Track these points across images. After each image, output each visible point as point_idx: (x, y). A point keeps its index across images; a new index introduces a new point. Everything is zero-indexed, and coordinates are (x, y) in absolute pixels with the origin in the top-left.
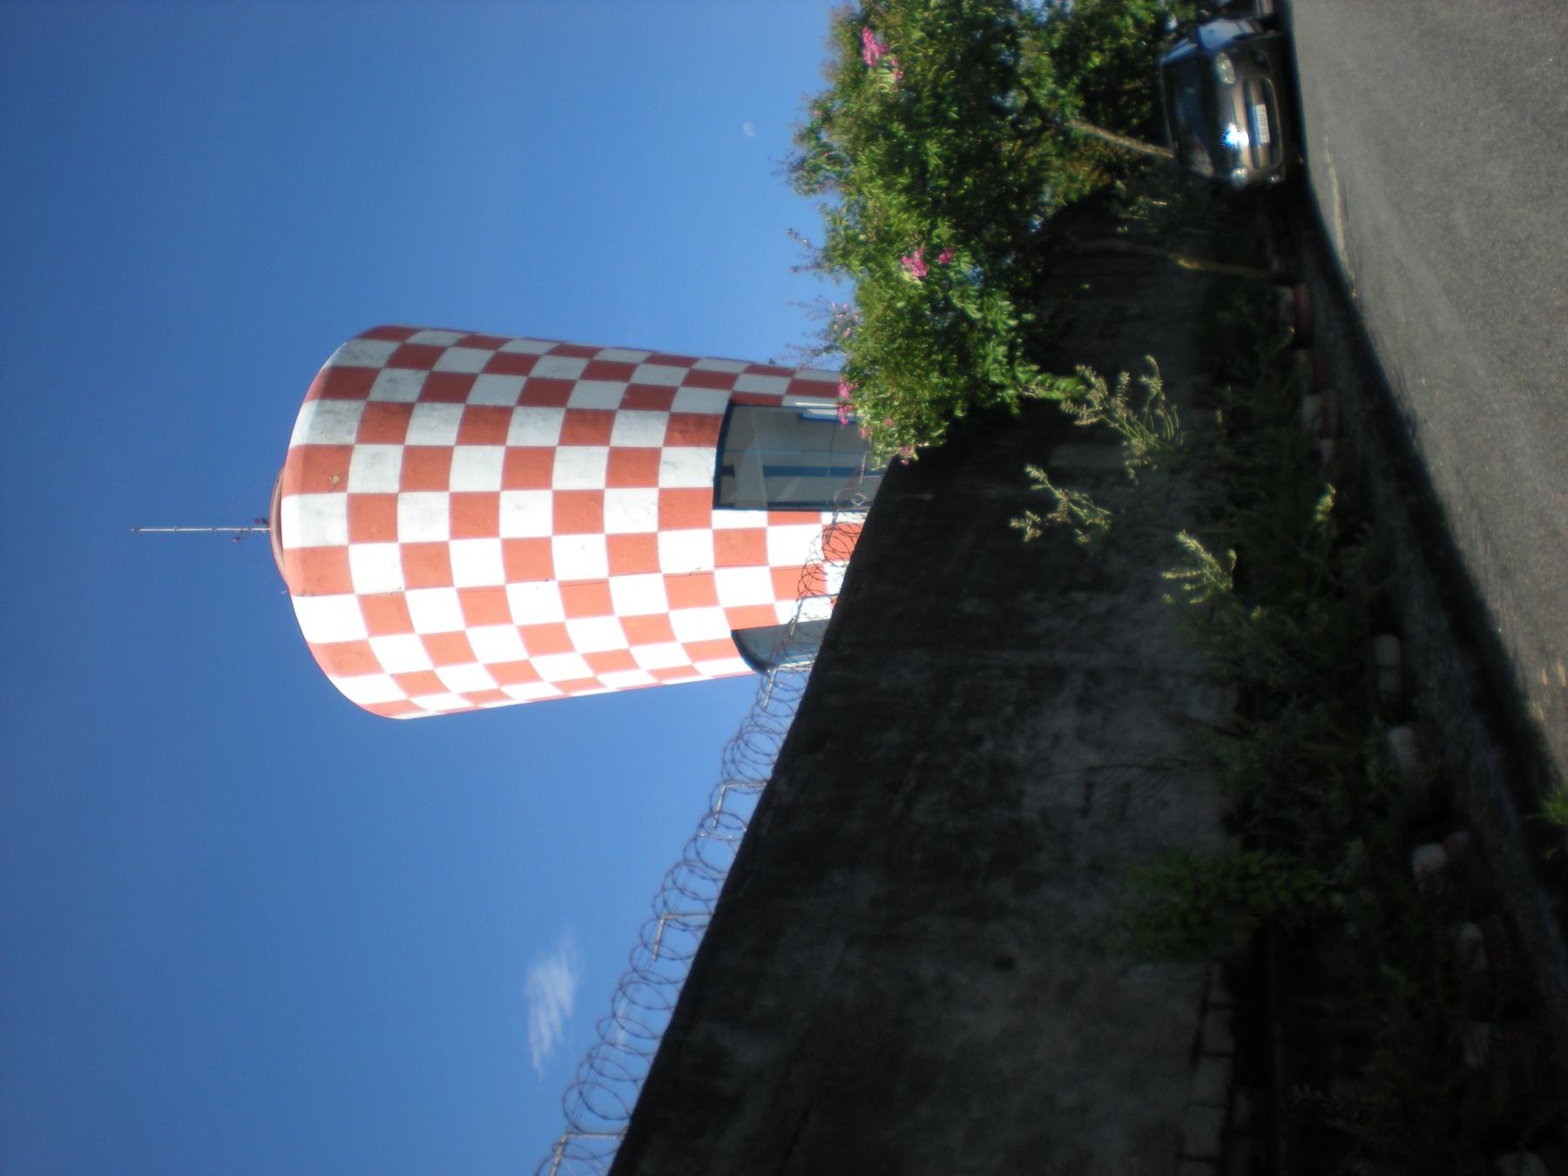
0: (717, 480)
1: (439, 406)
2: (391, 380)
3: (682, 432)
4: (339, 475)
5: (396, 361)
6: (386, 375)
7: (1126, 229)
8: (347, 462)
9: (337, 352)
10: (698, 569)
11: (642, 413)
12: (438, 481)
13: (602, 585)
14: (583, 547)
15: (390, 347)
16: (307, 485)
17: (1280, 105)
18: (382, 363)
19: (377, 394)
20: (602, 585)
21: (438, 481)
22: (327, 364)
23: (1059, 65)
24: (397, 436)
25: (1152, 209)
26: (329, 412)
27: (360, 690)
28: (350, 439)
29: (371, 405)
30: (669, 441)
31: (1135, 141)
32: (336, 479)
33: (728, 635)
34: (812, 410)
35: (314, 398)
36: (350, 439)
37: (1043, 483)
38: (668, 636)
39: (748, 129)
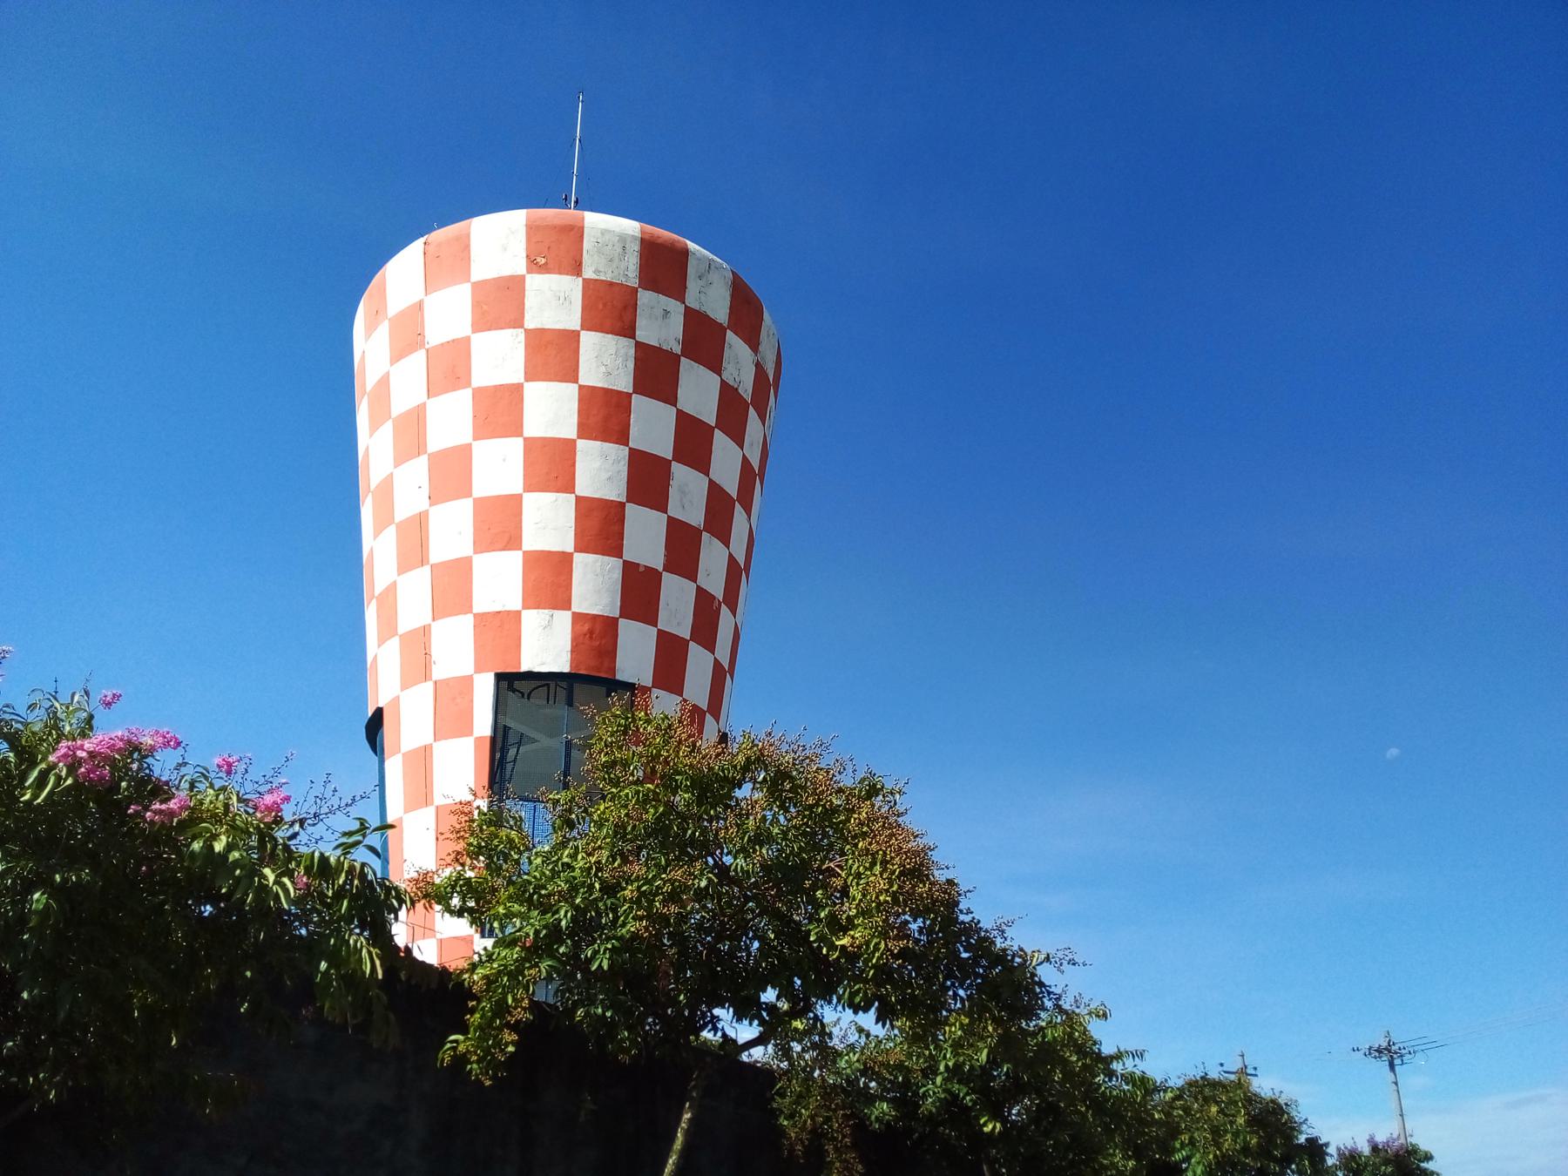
0: (530, 675)
2: (666, 312)
3: (591, 632)
11: (619, 587)
18: (692, 300)
22: (691, 245)
28: (588, 273)
30: (578, 618)
33: (380, 706)
35: (642, 232)
36: (588, 273)
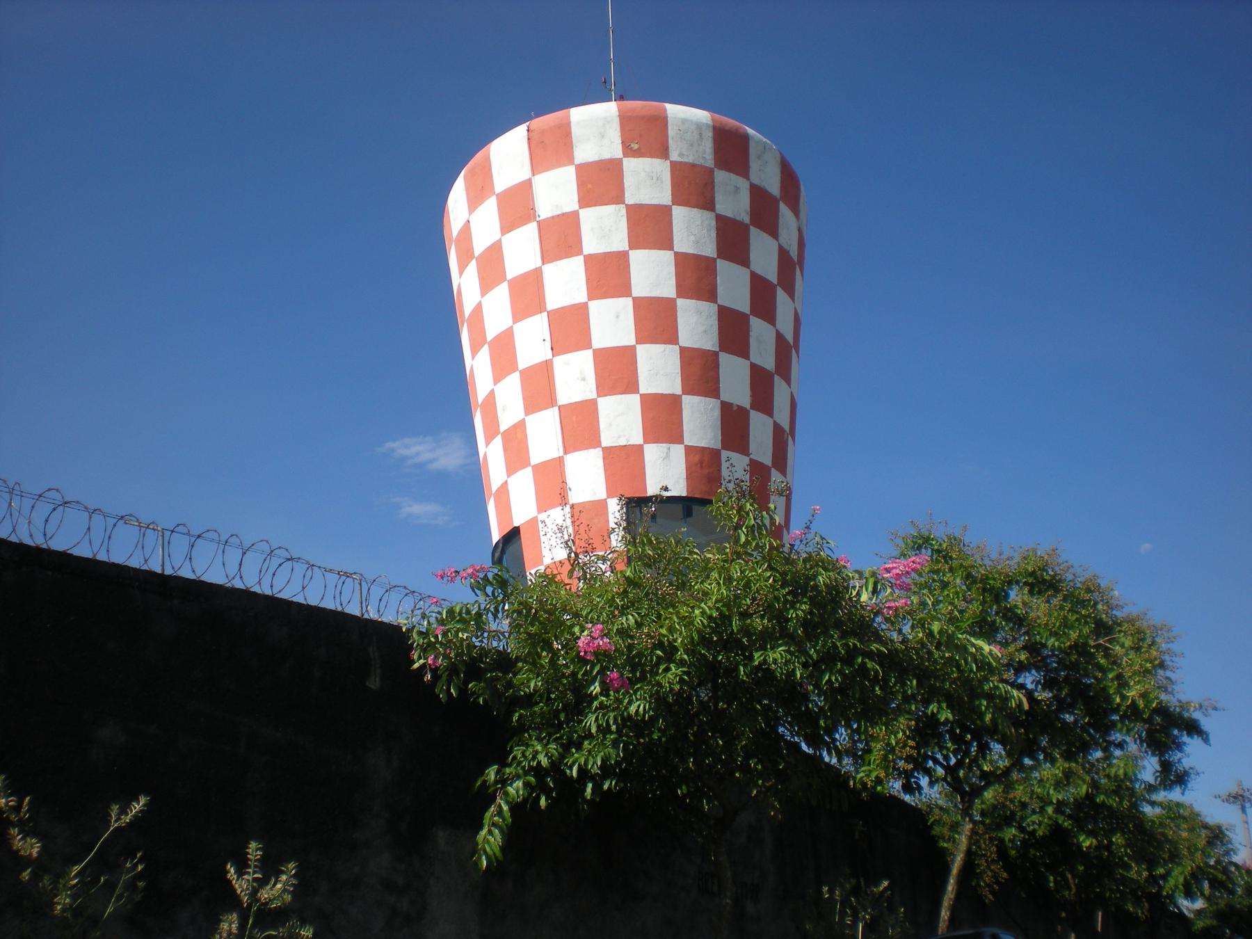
1: (714, 234)
3: (701, 462)
4: (639, 149)
5: (758, 193)
6: (744, 185)
7: (827, 896)
8: (651, 155)
9: (765, 140)
10: (570, 490)
12: (638, 239)
13: (551, 401)
14: (584, 379)
15: (774, 187)
16: (626, 121)
18: (754, 178)
19: (721, 176)
20: (551, 401)
21: (638, 239)
22: (750, 131)
23: (1079, 804)
24: (680, 197)
26: (701, 135)
27: (458, 196)
28: (674, 156)
29: (711, 172)
30: (689, 450)
31: (952, 896)
32: (635, 146)
33: (516, 525)
35: (713, 120)
36: (674, 156)
37: (118, 819)
38: (511, 469)
39: (1146, 547)
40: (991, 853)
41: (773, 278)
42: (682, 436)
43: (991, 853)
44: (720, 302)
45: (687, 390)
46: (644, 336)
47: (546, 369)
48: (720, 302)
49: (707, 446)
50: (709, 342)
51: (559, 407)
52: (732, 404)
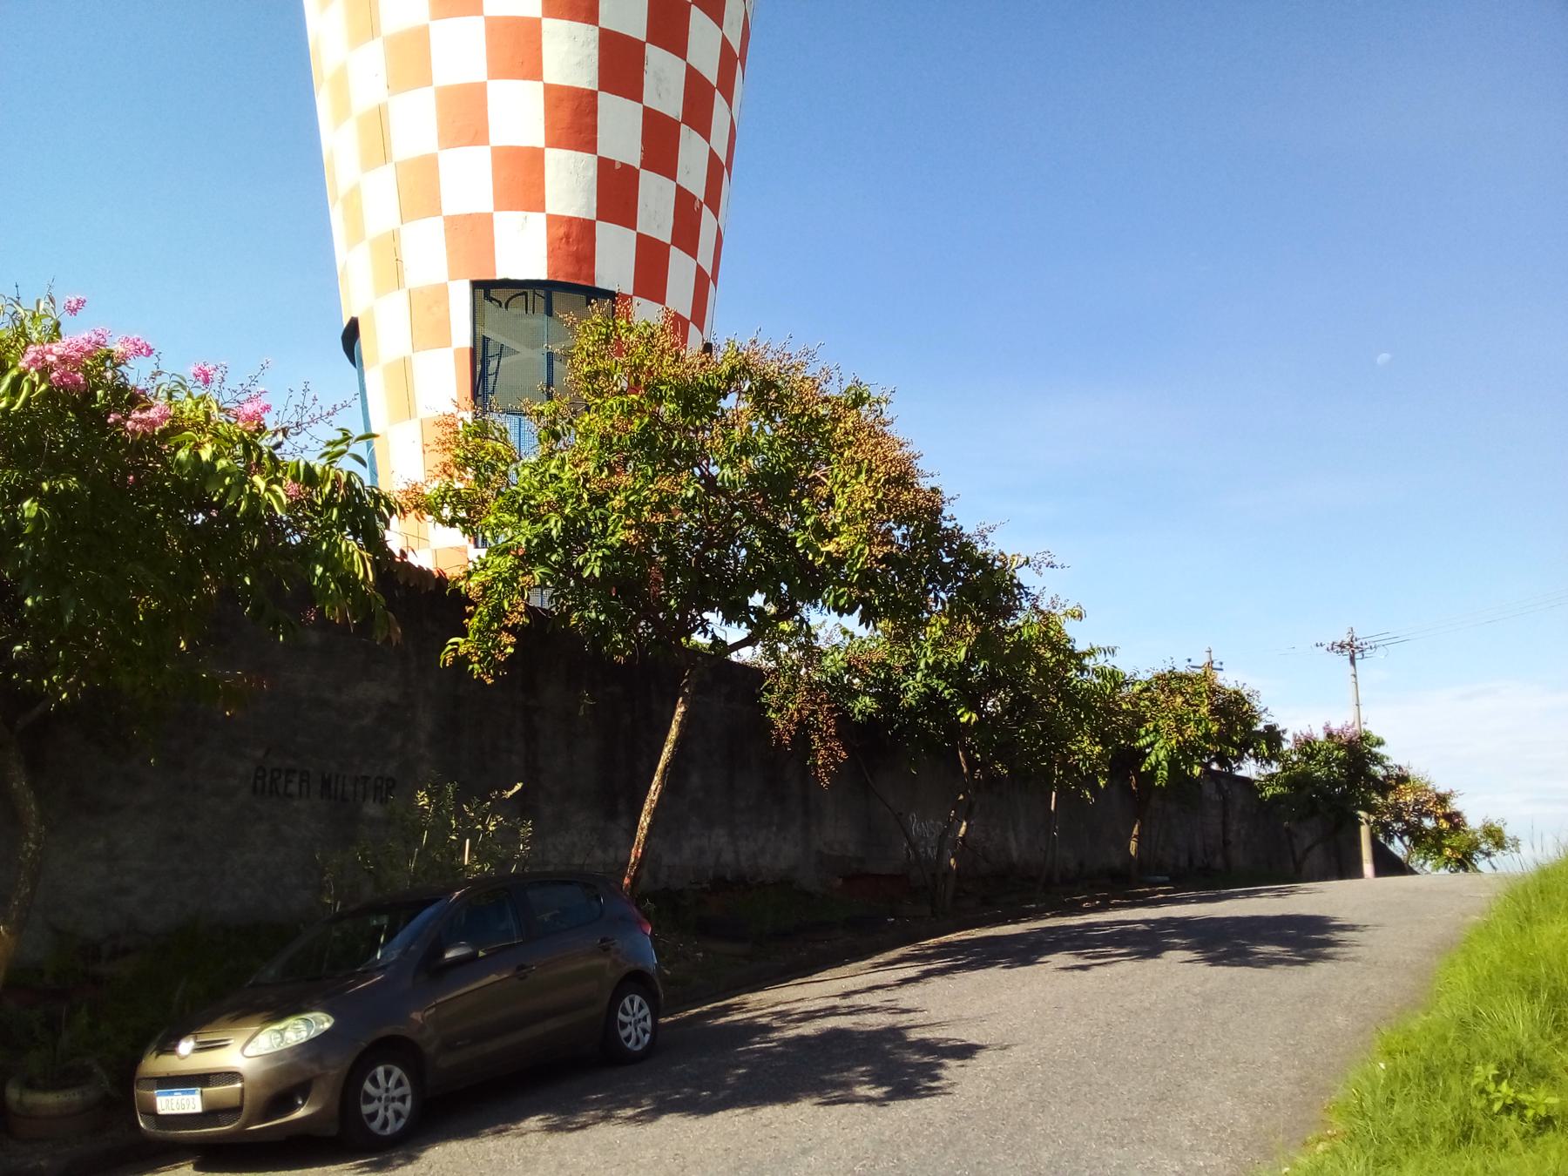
3: (567, 236)
17: (219, 1131)
25: (740, 1076)
30: (553, 220)
34: (757, 1020)
40: (829, 727)
41: (712, 77)
42: (543, 202)
43: (829, 727)
44: (602, 24)
45: (553, 143)
46: (500, 69)
47: (428, 166)
48: (602, 24)
49: (576, 216)
50: (585, 76)
51: (386, 158)
52: (614, 161)
